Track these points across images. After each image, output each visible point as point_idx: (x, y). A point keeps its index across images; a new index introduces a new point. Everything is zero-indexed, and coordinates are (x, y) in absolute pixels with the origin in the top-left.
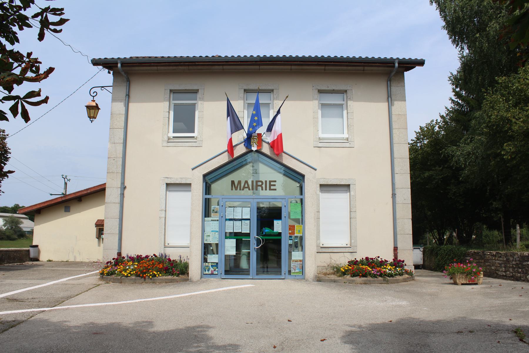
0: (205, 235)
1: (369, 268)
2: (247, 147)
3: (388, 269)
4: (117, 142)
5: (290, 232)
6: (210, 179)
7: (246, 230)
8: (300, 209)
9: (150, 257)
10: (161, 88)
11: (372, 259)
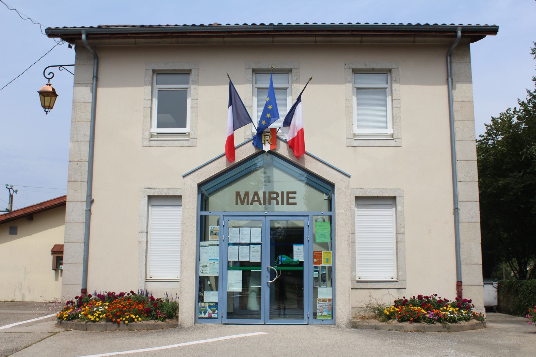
0: (201, 265)
1: (423, 311)
3: (449, 312)
5: (315, 260)
6: (206, 190)
8: (329, 230)
9: (126, 295)
10: (141, 67)
11: (427, 297)
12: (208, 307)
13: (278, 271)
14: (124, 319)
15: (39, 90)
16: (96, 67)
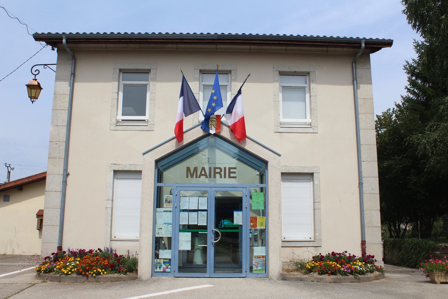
0: (157, 228)
1: (338, 265)
2: (204, 130)
3: (359, 265)
4: (61, 124)
5: (252, 224)
6: (163, 165)
7: (202, 222)
8: (263, 199)
9: (94, 252)
10: (110, 67)
11: (340, 254)
12: (162, 263)
13: (222, 233)
14: (92, 273)
15: (26, 84)
16: (73, 66)
